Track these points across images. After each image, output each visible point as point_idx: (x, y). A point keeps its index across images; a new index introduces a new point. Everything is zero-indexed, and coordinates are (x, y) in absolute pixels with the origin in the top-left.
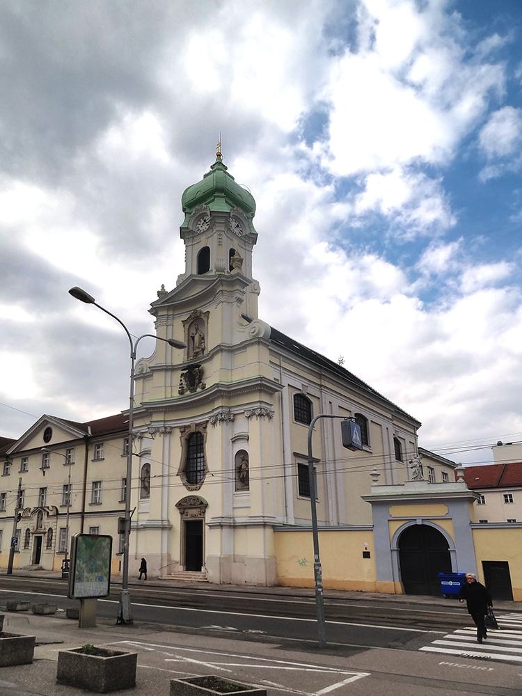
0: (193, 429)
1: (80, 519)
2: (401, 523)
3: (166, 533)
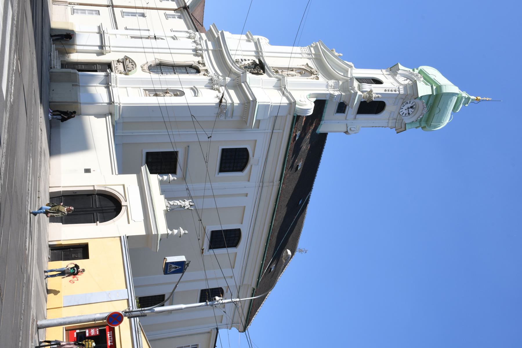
0: (201, 67)
1: (106, 4)
2: (122, 193)
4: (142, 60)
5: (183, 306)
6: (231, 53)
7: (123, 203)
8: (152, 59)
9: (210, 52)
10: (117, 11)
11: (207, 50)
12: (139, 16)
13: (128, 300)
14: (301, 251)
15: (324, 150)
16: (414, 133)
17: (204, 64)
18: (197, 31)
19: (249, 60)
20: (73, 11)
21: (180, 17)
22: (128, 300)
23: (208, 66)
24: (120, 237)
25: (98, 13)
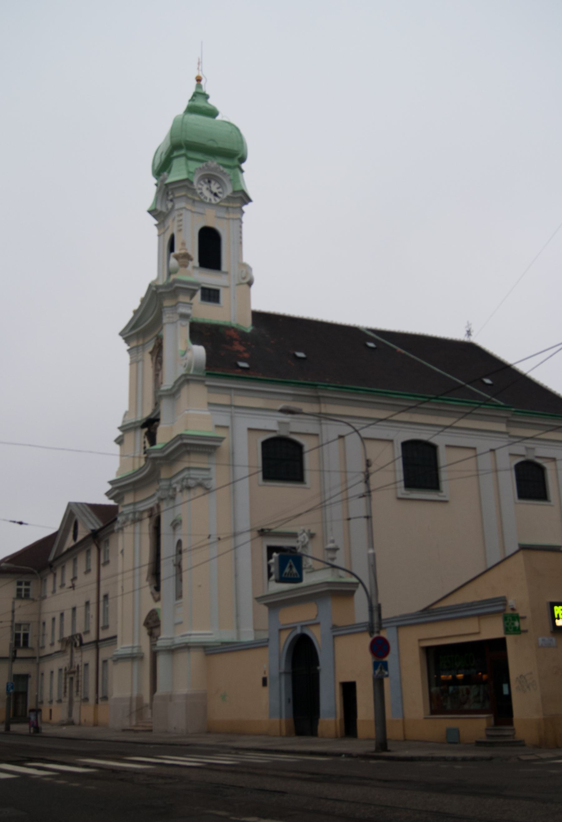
3: (136, 664)
4: (149, 604)
5: (438, 370)
6: (137, 467)
7: (299, 631)
8: (147, 590)
9: (139, 499)
10: (102, 636)
11: (134, 504)
12: (108, 603)
13: (398, 627)
14: (469, 333)
15: (136, 304)
16: (251, 177)
17: (151, 509)
18: (116, 519)
19: (145, 442)
20: (105, 698)
21: (107, 542)
22: (398, 627)
23: (151, 503)
24: (334, 637)
25: (105, 662)
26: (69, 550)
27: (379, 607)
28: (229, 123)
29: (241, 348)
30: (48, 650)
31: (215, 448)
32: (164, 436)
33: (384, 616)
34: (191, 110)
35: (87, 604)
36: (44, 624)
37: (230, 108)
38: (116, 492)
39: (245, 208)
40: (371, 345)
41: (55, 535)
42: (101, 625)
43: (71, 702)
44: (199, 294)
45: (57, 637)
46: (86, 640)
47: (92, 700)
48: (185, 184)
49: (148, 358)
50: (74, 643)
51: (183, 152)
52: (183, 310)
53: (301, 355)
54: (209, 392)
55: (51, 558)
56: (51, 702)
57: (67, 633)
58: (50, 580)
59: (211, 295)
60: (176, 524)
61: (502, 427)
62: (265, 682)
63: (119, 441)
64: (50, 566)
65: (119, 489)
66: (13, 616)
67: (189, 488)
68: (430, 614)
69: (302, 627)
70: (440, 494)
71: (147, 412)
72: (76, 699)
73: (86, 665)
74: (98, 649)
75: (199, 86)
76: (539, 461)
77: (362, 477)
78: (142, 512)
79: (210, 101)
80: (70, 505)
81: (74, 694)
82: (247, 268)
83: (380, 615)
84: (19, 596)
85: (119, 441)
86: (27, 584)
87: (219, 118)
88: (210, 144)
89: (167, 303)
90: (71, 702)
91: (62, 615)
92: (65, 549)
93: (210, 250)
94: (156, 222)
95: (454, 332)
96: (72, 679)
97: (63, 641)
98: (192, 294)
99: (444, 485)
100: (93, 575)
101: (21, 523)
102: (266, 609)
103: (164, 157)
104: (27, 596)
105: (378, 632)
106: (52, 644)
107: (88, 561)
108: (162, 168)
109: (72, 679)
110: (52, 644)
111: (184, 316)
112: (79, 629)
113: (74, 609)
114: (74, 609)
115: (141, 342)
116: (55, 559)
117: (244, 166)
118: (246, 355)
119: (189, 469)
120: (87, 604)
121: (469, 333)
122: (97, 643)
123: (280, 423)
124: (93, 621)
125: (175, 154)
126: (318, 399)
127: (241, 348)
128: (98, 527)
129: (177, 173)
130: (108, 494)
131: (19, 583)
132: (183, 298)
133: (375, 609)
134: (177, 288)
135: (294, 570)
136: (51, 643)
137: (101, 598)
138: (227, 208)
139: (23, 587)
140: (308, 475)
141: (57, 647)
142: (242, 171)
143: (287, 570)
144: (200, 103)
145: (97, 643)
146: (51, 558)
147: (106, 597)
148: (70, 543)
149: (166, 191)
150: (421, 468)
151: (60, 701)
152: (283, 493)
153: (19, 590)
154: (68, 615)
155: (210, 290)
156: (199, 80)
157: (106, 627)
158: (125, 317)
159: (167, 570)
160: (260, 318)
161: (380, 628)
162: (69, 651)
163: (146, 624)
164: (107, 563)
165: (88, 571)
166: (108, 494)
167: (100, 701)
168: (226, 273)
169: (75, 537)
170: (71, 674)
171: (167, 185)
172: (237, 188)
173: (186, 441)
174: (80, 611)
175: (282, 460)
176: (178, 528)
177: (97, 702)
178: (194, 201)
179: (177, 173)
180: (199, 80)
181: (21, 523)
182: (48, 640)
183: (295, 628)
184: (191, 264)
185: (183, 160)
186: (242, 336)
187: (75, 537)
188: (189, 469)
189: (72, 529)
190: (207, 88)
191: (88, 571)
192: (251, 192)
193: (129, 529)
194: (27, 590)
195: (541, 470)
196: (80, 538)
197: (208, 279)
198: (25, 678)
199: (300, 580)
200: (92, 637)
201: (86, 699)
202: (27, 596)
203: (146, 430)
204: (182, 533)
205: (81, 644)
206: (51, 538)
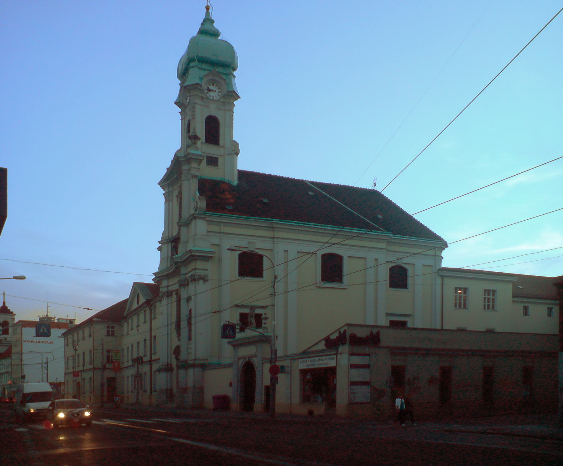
8: (175, 334)
9: (170, 283)
10: (154, 358)
11: (168, 286)
14: (375, 184)
22: (291, 359)
26: (134, 310)
27: (276, 351)
28: (226, 42)
29: (229, 196)
30: (126, 365)
31: (211, 257)
32: (181, 250)
33: (278, 356)
34: (202, 32)
35: (145, 340)
36: (123, 350)
37: (227, 32)
38: (158, 279)
39: (235, 103)
40: (311, 193)
41: (127, 300)
42: (152, 352)
43: (138, 393)
44: (204, 161)
45: (130, 358)
46: (145, 359)
47: (149, 391)
48: (196, 86)
49: (175, 199)
50: (138, 361)
51: (196, 63)
52: (193, 172)
53: (265, 200)
54: (208, 224)
55: (125, 314)
56: (128, 392)
57: (135, 356)
58: (125, 325)
59: (213, 161)
60: (189, 299)
61: (383, 246)
62: (231, 384)
63: (159, 249)
64: (125, 318)
65: (158, 277)
66: (103, 347)
67: (195, 280)
68: (305, 354)
69: (249, 357)
70: (342, 285)
71: (175, 233)
72: (141, 391)
73: (145, 373)
74: (151, 364)
75: (208, 13)
76: (404, 265)
77: (271, 285)
78: (171, 292)
79: (214, 25)
80: (135, 284)
81: (140, 388)
82: (236, 145)
83: (276, 354)
84: (108, 334)
85: (159, 249)
86: (113, 327)
87: (219, 38)
88: (214, 58)
89: (185, 167)
90: (138, 393)
91: (132, 345)
92: (132, 309)
93: (214, 130)
94: (180, 110)
95: (365, 184)
96: (138, 380)
97: (133, 360)
98: (200, 161)
99: (345, 279)
100: (148, 324)
101: (88, 309)
102: (232, 348)
103: (184, 66)
104: (113, 335)
105: (274, 363)
106: (128, 361)
107: (145, 316)
108: (183, 74)
109: (138, 380)
110: (128, 361)
111: (194, 176)
112: (141, 354)
113: (138, 343)
114: (138, 343)
115: (171, 189)
116: (128, 314)
117: (235, 73)
118: (232, 201)
119: (195, 269)
120: (145, 340)
121: (375, 184)
122: (150, 362)
123: (249, 243)
124: (148, 350)
125: (192, 64)
126: (273, 229)
127: (229, 196)
128: (150, 298)
129: (194, 77)
130: (153, 280)
131: (108, 327)
132: (194, 165)
133: (274, 352)
134: (190, 158)
135: (231, 332)
136: (127, 361)
137: (153, 337)
138: (224, 102)
139: (111, 329)
140: (265, 273)
141: (130, 363)
142: (234, 77)
143: (227, 332)
144: (207, 27)
145: (150, 362)
146: (125, 314)
147: (155, 337)
148: (135, 306)
149: (185, 89)
150: (332, 269)
151: (132, 392)
152: (251, 282)
153: (108, 331)
154: (135, 345)
155: (212, 158)
156: (208, 8)
157: (155, 353)
158: (162, 173)
159: (184, 324)
160: (243, 175)
161: (276, 360)
162: (136, 364)
163: (174, 353)
164: (155, 318)
165: (145, 322)
166: (153, 280)
167: (153, 393)
168: (223, 146)
169: (138, 302)
170: (138, 377)
171: (185, 87)
172: (230, 90)
173: (193, 254)
174: (142, 344)
175: (251, 265)
176: (190, 302)
177: (151, 393)
178: (202, 98)
179: (194, 77)
180: (208, 8)
181: (88, 309)
182: (125, 360)
183: (245, 358)
184: (199, 142)
185: (196, 69)
186: (231, 188)
187: (138, 302)
188: (195, 269)
189: (136, 297)
190: (214, 15)
191: (145, 322)
192: (239, 92)
193: (165, 301)
194: (113, 331)
195: (405, 271)
196: (140, 304)
197: (212, 150)
198: (113, 379)
199: (234, 337)
200: (146, 359)
201: (146, 391)
202: (113, 335)
203: (174, 244)
204: (192, 305)
205: (143, 362)
206: (124, 302)
